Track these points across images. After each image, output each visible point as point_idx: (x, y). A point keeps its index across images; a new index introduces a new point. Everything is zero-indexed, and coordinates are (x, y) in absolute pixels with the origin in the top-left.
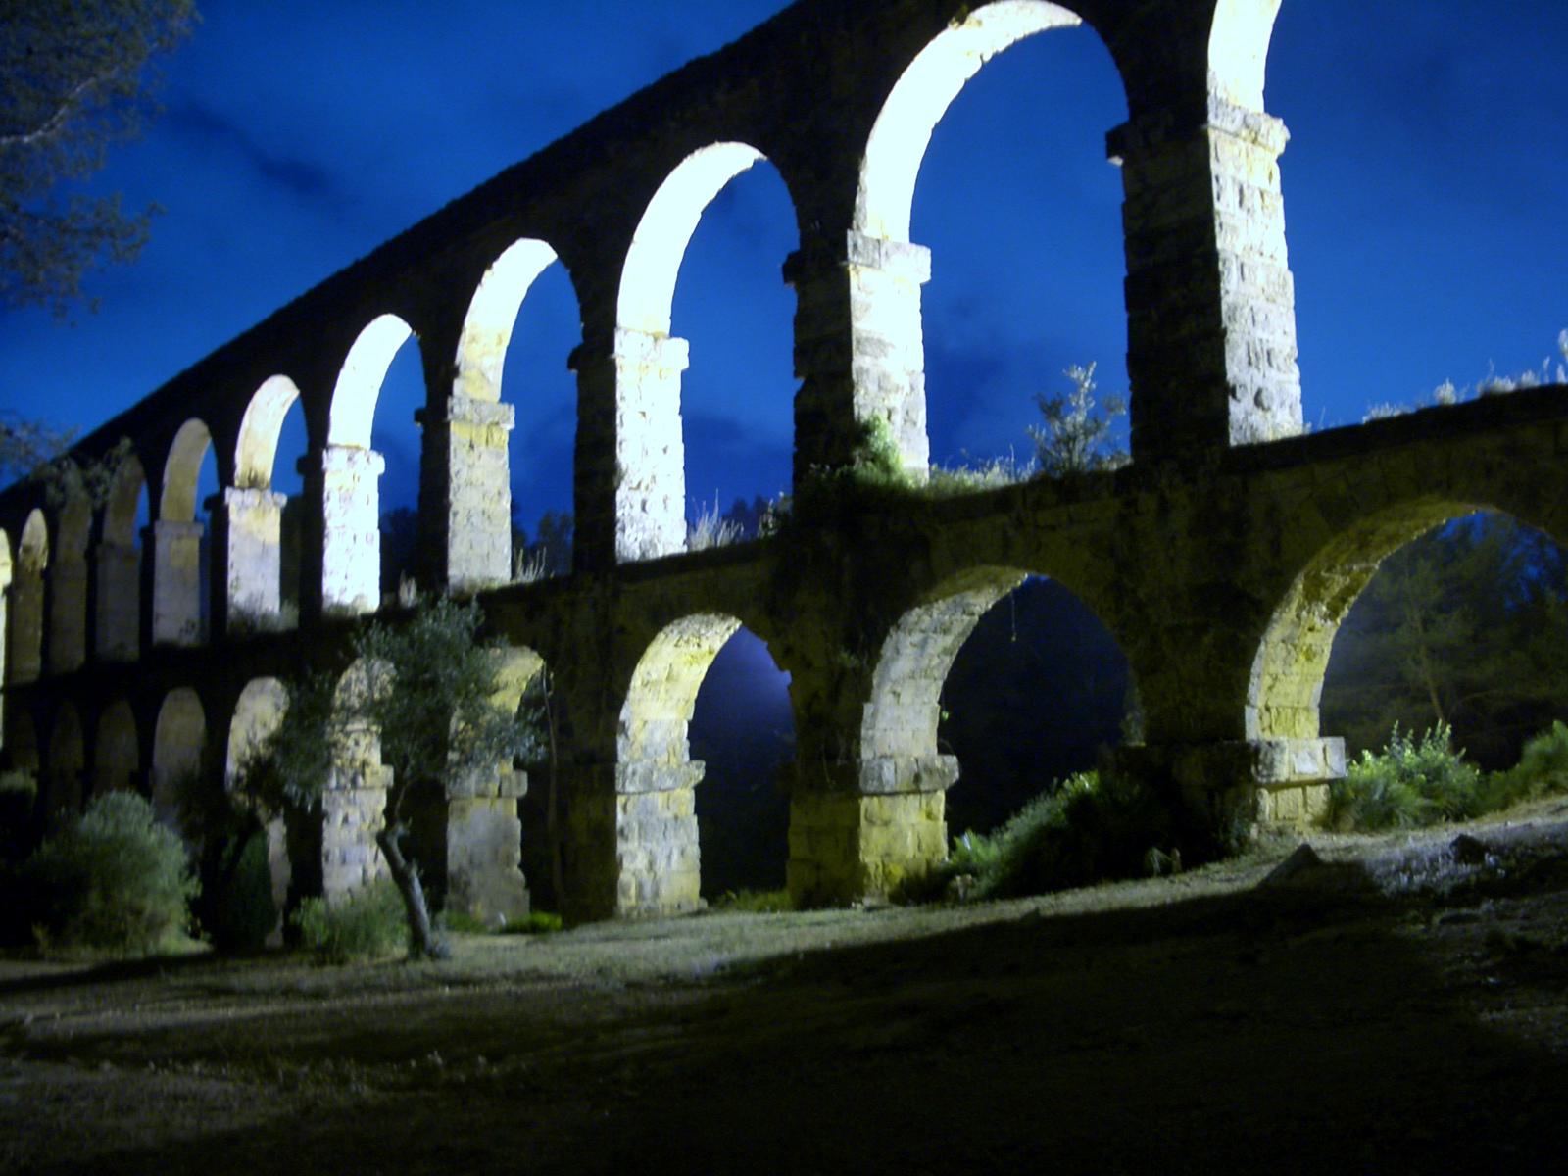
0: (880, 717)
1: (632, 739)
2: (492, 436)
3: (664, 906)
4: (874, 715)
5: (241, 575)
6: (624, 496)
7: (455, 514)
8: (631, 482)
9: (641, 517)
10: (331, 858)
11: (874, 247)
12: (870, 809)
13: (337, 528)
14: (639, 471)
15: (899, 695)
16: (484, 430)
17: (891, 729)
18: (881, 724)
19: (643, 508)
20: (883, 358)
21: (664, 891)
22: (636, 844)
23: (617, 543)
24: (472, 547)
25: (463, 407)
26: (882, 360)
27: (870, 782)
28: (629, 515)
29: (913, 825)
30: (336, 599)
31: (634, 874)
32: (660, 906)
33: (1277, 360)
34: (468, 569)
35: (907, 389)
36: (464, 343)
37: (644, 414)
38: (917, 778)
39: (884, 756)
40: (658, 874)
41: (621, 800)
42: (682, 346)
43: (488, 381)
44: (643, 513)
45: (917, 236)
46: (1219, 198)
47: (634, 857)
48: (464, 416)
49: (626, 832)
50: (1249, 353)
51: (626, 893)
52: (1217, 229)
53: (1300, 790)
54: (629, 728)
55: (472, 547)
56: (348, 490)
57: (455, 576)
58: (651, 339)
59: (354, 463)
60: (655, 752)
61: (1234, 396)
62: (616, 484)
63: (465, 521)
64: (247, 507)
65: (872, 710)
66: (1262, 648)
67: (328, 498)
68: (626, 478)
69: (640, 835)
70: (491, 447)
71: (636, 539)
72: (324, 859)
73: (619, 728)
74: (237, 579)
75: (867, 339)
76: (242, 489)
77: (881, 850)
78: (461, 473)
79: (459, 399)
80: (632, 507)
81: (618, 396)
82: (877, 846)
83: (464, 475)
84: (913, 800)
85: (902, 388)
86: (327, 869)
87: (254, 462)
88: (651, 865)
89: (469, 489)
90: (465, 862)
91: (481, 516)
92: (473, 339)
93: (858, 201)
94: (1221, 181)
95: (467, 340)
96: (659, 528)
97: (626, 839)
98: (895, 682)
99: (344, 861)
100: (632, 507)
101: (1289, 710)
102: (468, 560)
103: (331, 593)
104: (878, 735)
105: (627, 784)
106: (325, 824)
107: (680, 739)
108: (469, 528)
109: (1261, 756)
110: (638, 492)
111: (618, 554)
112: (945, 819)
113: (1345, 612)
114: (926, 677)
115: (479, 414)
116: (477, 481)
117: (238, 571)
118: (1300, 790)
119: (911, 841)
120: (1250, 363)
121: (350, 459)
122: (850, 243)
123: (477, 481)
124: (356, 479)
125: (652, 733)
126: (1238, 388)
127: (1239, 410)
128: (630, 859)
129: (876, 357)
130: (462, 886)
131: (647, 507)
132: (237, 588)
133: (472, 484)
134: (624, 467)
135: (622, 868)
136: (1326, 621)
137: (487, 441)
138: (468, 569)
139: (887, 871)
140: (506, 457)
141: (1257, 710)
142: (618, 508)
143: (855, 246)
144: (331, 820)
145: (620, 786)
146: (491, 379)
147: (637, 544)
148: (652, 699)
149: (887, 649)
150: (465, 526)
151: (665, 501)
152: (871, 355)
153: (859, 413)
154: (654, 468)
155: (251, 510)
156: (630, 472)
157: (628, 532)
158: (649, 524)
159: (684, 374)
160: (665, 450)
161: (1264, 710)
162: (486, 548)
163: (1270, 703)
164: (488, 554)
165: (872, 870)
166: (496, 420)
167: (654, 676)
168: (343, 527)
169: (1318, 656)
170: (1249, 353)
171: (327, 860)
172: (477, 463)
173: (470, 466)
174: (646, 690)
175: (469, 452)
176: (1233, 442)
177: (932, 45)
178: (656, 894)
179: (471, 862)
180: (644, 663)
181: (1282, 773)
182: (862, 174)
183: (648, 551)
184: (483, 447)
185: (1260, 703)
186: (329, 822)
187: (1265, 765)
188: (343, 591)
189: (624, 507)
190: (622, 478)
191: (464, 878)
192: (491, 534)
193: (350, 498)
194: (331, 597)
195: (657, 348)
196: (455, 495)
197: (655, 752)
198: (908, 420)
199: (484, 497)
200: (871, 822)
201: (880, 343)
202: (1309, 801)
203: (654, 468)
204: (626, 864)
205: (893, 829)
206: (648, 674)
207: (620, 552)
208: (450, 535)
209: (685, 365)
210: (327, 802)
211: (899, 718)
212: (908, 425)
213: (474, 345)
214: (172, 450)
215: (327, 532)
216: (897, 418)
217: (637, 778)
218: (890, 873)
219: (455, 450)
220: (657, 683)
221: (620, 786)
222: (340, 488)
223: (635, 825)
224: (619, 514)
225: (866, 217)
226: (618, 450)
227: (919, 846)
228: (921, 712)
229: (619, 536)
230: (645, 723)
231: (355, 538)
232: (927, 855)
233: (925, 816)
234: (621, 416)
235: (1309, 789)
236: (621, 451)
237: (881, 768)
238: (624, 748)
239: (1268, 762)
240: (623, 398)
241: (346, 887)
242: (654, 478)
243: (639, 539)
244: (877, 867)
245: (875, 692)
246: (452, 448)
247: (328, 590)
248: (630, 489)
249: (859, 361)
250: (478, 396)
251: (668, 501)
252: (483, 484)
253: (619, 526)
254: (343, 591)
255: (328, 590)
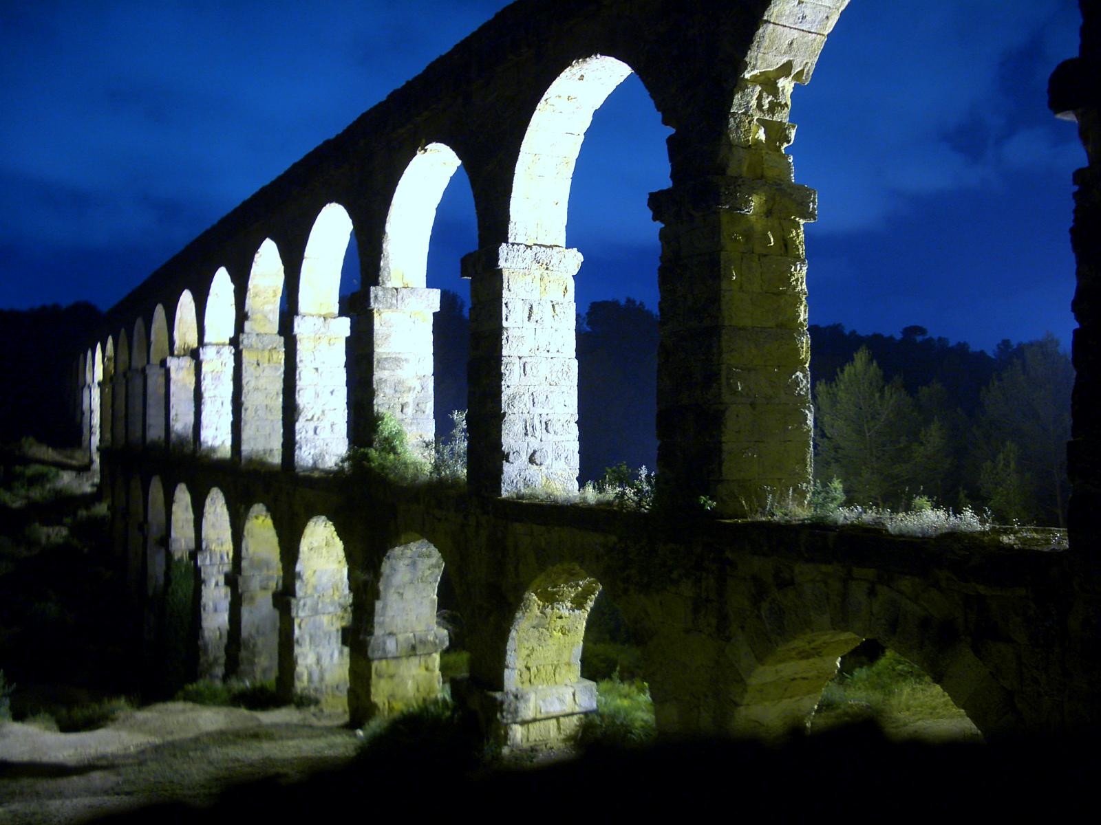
0: (388, 608)
1: (306, 582)
2: (272, 356)
3: (327, 687)
4: (384, 608)
5: (179, 412)
6: (301, 426)
7: (246, 410)
8: (306, 416)
9: (314, 439)
10: (207, 608)
11: (393, 295)
12: (379, 668)
13: (210, 397)
14: (312, 408)
15: (402, 594)
16: (266, 354)
17: (398, 615)
18: (390, 613)
19: (315, 432)
20: (399, 370)
21: (328, 677)
22: (308, 647)
23: (296, 457)
24: (258, 430)
25: (250, 340)
26: (399, 372)
27: (376, 652)
28: (305, 438)
29: (414, 677)
30: (210, 444)
31: (306, 667)
32: (324, 687)
33: (555, 426)
34: (255, 445)
35: (419, 388)
36: (249, 298)
37: (317, 369)
38: (414, 648)
39: (391, 634)
40: (323, 667)
41: (297, 622)
42: (346, 322)
43: (269, 320)
44: (315, 436)
45: (430, 284)
46: (507, 319)
47: (306, 657)
48: (251, 346)
49: (300, 641)
50: (526, 427)
51: (300, 679)
52: (504, 342)
53: (554, 721)
54: (303, 575)
55: (258, 430)
56: (217, 372)
57: (246, 450)
58: (323, 319)
59: (221, 355)
60: (323, 589)
61: (508, 461)
62: (296, 418)
63: (253, 414)
64: (182, 368)
65: (381, 605)
66: (513, 633)
67: (204, 379)
68: (302, 414)
69: (311, 643)
70: (272, 364)
71: (310, 453)
72: (202, 609)
73: (297, 576)
74: (176, 415)
75: (386, 359)
76: (178, 357)
77: (386, 694)
78: (250, 383)
79: (249, 334)
80: (307, 432)
81: (298, 360)
82: (383, 691)
83: (252, 384)
84: (415, 660)
85: (415, 388)
86: (204, 615)
87: (187, 338)
88: (318, 661)
89: (255, 393)
90: (253, 632)
91: (265, 409)
92: (256, 295)
93: (382, 264)
94: (509, 305)
95: (252, 296)
96: (327, 445)
97: (300, 645)
98: (398, 587)
99: (216, 610)
100: (307, 432)
101: (550, 667)
102: (255, 439)
103: (206, 440)
104: (387, 620)
105: (300, 612)
106: (203, 587)
107: (341, 579)
108: (256, 418)
109: (505, 706)
110: (312, 422)
111: (296, 464)
112: (440, 670)
113: (590, 604)
114: (422, 582)
115: (262, 343)
116: (262, 386)
117: (177, 411)
118: (554, 721)
119: (410, 685)
120: (526, 434)
121: (218, 352)
122: (372, 295)
123: (262, 386)
124: (223, 365)
125: (320, 577)
126: (511, 454)
127: (510, 471)
128: (302, 658)
129: (393, 370)
130: (251, 646)
131: (318, 432)
132: (176, 420)
133: (258, 389)
134: (301, 406)
135: (297, 663)
136: (573, 611)
137: (269, 360)
138: (255, 445)
139: (391, 706)
140: (282, 369)
141: (516, 671)
142: (297, 434)
143: (376, 297)
144: (207, 585)
145: (295, 613)
146: (271, 319)
147: (310, 456)
148: (318, 557)
149: (385, 568)
150: (253, 417)
151: (332, 426)
152: (389, 370)
153: (378, 410)
154: (324, 405)
155: (185, 370)
156: (305, 409)
157: (304, 449)
158: (319, 443)
159: (348, 340)
160: (332, 393)
161: (524, 670)
162: (268, 430)
163: (529, 665)
164: (270, 434)
165: (381, 705)
166: (275, 346)
167: (315, 545)
168: (215, 397)
169: (572, 633)
170: (526, 427)
171: (204, 609)
172: (262, 375)
173: (256, 377)
174: (312, 552)
175: (255, 368)
176: (504, 494)
177: (411, 163)
178: (322, 679)
179: (258, 632)
180: (306, 537)
181: (528, 712)
182: (384, 246)
183: (318, 460)
184: (266, 365)
185: (520, 664)
186: (205, 585)
187: (509, 712)
188: (215, 438)
189: (301, 433)
190: (299, 414)
191: (252, 641)
192: (272, 421)
193: (219, 377)
194: (207, 442)
195: (326, 326)
196: (245, 397)
197: (323, 589)
198: (418, 408)
199: (266, 397)
200: (380, 676)
201: (397, 360)
202: (562, 727)
203: (324, 405)
204: (300, 661)
205: (396, 680)
206: (311, 543)
207: (298, 462)
208: (242, 424)
209: (348, 334)
210: (204, 573)
211: (404, 608)
212: (419, 413)
213: (257, 298)
214: (154, 321)
215: (203, 401)
216: (409, 410)
217: (306, 608)
218: (393, 708)
219: (246, 368)
220: (319, 548)
221: (295, 613)
222: (213, 372)
223: (307, 638)
224: (298, 437)
225: (389, 274)
226: (297, 396)
227: (418, 690)
228: (422, 603)
229: (297, 452)
230: (315, 572)
231: (222, 404)
232: (424, 694)
233: (424, 669)
234: (300, 374)
235: (562, 719)
236: (299, 396)
237: (385, 643)
238: (300, 587)
239: (512, 709)
240: (301, 361)
241: (216, 626)
242: (323, 412)
243: (312, 453)
244: (384, 704)
245: (382, 594)
246: (244, 366)
247: (204, 438)
248: (307, 420)
249: (378, 375)
250: (262, 331)
251: (334, 426)
252: (266, 389)
253: (297, 446)
254: (215, 438)
255: (204, 438)
